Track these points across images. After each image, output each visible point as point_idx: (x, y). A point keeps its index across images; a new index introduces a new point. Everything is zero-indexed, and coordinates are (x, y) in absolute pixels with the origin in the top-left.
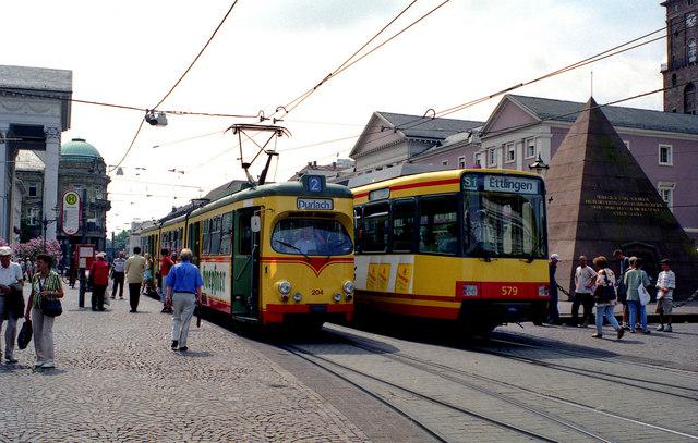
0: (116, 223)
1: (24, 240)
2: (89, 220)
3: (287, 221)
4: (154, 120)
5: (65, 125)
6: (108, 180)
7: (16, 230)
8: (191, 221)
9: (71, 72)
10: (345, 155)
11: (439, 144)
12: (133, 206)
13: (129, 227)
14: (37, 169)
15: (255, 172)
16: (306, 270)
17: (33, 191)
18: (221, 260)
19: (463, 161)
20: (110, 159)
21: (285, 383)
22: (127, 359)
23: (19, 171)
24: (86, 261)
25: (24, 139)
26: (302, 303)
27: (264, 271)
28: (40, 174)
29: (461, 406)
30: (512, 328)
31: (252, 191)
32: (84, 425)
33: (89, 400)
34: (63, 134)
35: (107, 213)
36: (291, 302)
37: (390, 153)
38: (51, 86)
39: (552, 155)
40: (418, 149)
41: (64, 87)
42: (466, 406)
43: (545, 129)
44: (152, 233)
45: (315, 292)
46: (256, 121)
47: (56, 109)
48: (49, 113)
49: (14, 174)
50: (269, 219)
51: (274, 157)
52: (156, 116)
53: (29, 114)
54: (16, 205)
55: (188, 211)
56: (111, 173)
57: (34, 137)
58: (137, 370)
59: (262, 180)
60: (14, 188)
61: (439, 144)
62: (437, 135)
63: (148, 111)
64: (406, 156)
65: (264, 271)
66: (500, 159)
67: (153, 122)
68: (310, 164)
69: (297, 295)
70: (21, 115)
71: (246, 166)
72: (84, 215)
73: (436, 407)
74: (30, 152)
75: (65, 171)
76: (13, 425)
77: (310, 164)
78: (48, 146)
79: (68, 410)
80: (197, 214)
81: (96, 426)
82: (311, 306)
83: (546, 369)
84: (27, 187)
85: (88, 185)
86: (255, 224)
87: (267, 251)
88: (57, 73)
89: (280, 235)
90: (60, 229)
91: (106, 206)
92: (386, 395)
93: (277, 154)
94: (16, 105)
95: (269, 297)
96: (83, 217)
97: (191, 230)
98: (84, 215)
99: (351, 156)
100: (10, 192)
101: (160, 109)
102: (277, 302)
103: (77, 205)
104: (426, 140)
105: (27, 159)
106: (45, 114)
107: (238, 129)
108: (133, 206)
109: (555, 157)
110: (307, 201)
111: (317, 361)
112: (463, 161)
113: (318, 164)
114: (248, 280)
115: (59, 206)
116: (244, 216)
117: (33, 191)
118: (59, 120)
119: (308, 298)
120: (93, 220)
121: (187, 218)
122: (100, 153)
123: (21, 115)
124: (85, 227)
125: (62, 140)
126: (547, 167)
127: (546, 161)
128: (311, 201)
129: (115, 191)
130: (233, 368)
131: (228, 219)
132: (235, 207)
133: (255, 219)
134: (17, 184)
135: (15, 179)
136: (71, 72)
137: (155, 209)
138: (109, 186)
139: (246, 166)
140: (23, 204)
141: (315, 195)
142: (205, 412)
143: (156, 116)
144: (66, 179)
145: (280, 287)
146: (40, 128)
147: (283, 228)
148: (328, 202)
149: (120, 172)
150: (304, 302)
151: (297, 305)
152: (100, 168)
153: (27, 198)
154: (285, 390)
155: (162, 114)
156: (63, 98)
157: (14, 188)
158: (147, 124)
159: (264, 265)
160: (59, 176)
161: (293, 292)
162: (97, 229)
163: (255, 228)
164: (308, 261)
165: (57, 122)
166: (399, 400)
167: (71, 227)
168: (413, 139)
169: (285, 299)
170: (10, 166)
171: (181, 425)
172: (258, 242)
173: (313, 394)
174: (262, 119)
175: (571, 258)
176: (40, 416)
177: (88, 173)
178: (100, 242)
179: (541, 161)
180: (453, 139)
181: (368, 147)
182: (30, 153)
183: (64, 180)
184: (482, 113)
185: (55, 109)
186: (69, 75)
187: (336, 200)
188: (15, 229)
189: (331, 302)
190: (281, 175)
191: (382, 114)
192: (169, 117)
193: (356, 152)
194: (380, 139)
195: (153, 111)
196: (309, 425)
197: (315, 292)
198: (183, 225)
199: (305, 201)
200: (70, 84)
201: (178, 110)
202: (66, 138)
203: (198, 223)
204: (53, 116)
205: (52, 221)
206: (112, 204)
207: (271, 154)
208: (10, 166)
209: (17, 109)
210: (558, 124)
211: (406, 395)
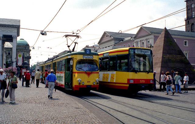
0: (32, 62)
1: (7, 67)
2: (25, 62)
3: (80, 62)
4: (43, 34)
5: (18, 35)
6: (30, 50)
7: (4, 64)
8: (53, 62)
9: (20, 20)
10: (96, 44)
11: (123, 40)
12: (37, 58)
13: (36, 64)
14: (10, 47)
15: (71, 48)
16: (85, 76)
17: (9, 54)
18: (62, 73)
19: (129, 45)
20: (31, 45)
21: (80, 107)
22: (35, 100)
23: (5, 48)
24: (24, 73)
25: (7, 39)
26: (84, 85)
27: (74, 76)
28: (11, 49)
29: (129, 114)
30: (143, 92)
31: (70, 54)
32: (24, 119)
33: (25, 112)
34: (18, 38)
35: (30, 60)
36: (81, 85)
37: (109, 43)
38: (14, 24)
39: (154, 43)
40: (117, 42)
41: (18, 24)
42: (130, 114)
43: (152, 36)
44: (42, 65)
45: (88, 82)
46: (72, 34)
47: (16, 31)
48: (14, 32)
49: (4, 49)
50: (75, 61)
51: (76, 44)
52: (44, 33)
53: (8, 32)
54: (5, 57)
55: (53, 59)
56: (31, 48)
57: (9, 38)
58: (38, 104)
59: (73, 50)
60: (4, 52)
61: (123, 40)
62: (122, 38)
63: (41, 31)
64: (113, 44)
65: (74, 76)
66: (140, 44)
67: (43, 34)
68: (87, 46)
69: (83, 82)
70: (6, 32)
71: (69, 46)
72: (23, 60)
73: (122, 114)
74: (8, 43)
75: (18, 48)
76: (4, 119)
77: (87, 46)
78: (13, 41)
79: (19, 115)
80: (55, 60)
81: (27, 119)
82: (87, 86)
83: (153, 103)
84: (8, 52)
85: (25, 52)
86: (71, 63)
87: (75, 70)
88: (16, 20)
89: (78, 66)
90: (17, 64)
91: (30, 58)
92: (108, 111)
93: (77, 43)
94: (4, 29)
95: (75, 83)
96: (23, 61)
97: (53, 64)
98: (23, 60)
99: (98, 44)
100: (3, 54)
101: (45, 30)
102: (77, 84)
103: (22, 57)
104: (119, 39)
105: (8, 45)
106: (13, 32)
107: (66, 36)
108: (37, 58)
109: (155, 44)
110: (86, 56)
111: (89, 101)
112: (129, 45)
113: (89, 46)
114: (69, 78)
115: (17, 58)
116: (68, 60)
117: (9, 54)
118: (16, 34)
119: (86, 84)
120: (26, 62)
121: (52, 61)
122: (28, 43)
123: (6, 32)
124: (24, 63)
125: (17, 39)
126: (153, 47)
127: (153, 45)
128: (87, 56)
129: (32, 53)
130: (65, 103)
131: (64, 61)
132: (66, 58)
133: (71, 61)
134: (5, 52)
135: (4, 50)
136: (20, 20)
137: (43, 59)
138: (31, 52)
139: (69, 46)
140: (7, 57)
141: (88, 55)
142: (57, 115)
143: (44, 33)
144: (18, 50)
145: (78, 80)
146: (11, 36)
147: (79, 64)
148: (92, 56)
149: (34, 48)
150: (85, 84)
151: (83, 85)
152: (28, 47)
153: (8, 55)
154: (80, 109)
155: (45, 32)
156: (18, 28)
157: (4, 52)
158: (41, 35)
159: (74, 74)
160: (17, 49)
161: (82, 82)
162: (27, 64)
163: (71, 64)
164: (86, 73)
165: (16, 34)
166: (112, 112)
167: (20, 63)
168: (115, 39)
169: (80, 84)
170: (3, 47)
171: (51, 119)
172: (72, 68)
173: (87, 110)
174: (73, 33)
175: (160, 72)
176: (11, 116)
177: (25, 48)
178: (28, 68)
179: (151, 45)
180: (127, 39)
181: (103, 41)
182: (8, 43)
183: (18, 50)
184: (135, 32)
185: (15, 30)
186: (19, 21)
187: (94, 56)
188: (4, 64)
189: (92, 85)
190: (79, 49)
191: (107, 32)
192: (47, 33)
193: (99, 43)
194: (106, 39)
195: (43, 31)
196: (86, 119)
197: (88, 82)
198: (51, 63)
199: (85, 56)
200: (20, 24)
201: (50, 31)
202: (19, 39)
203: (55, 63)
204: (15, 32)
205: (14, 62)
206: (31, 57)
207: (76, 43)
208: (3, 47)
209: (5, 31)
210: (156, 35)
211: (113, 111)
